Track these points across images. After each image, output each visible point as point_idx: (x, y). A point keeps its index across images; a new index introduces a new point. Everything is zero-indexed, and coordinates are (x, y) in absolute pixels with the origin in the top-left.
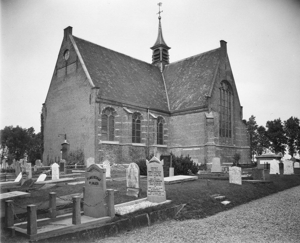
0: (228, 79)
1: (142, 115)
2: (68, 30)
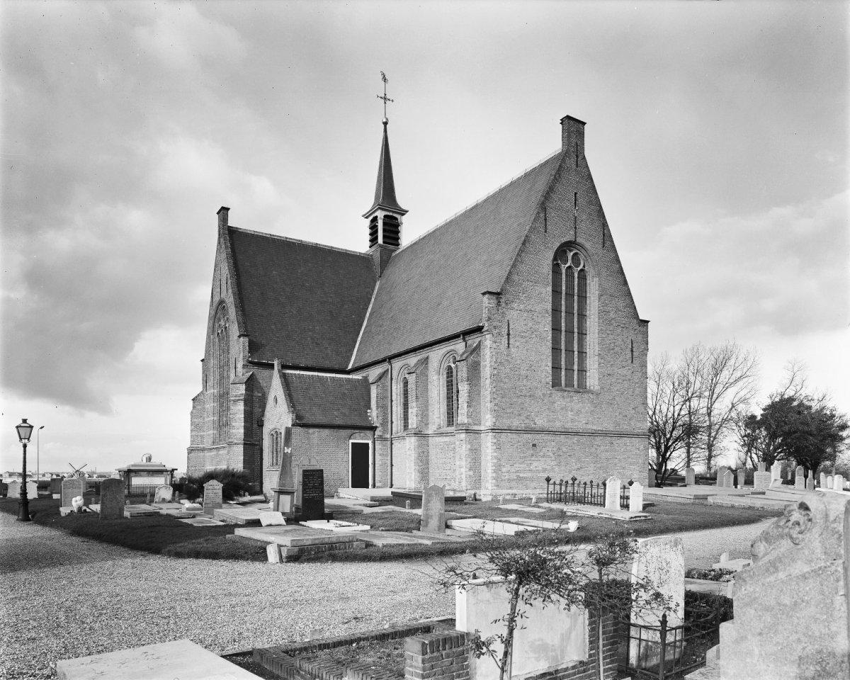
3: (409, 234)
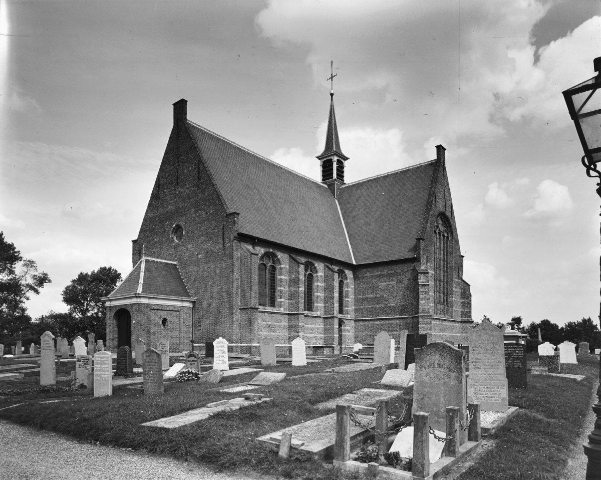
0: (448, 213)
2: (180, 107)
3: (351, 176)
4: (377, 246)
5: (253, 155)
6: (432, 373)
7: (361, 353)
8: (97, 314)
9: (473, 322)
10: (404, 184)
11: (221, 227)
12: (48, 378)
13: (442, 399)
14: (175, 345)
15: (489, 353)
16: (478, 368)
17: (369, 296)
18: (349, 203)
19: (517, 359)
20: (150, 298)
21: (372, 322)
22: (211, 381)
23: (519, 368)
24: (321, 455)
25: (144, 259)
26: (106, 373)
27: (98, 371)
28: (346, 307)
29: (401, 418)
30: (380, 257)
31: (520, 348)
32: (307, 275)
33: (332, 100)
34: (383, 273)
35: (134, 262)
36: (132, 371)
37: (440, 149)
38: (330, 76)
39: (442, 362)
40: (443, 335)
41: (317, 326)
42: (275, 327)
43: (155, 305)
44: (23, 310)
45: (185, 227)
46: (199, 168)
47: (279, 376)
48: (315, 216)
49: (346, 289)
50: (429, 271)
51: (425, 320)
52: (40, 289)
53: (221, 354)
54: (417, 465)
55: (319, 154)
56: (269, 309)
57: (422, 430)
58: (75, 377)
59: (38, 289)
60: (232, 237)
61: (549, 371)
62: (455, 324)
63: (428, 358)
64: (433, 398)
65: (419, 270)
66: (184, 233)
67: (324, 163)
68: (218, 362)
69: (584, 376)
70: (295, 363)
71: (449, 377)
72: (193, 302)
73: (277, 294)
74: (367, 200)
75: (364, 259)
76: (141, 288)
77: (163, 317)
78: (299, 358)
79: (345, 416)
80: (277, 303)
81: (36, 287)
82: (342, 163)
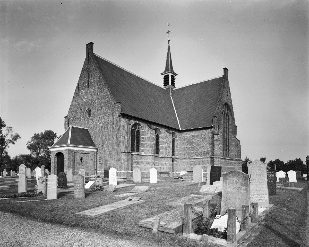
0: (229, 104)
1: (161, 130)
2: (90, 46)
3: (179, 84)
4: (192, 120)
5: (128, 73)
6: (232, 187)
7: (184, 176)
8: (44, 155)
9: (241, 160)
10: (207, 88)
11: (112, 110)
12: (22, 189)
13: (237, 201)
14: (87, 172)
15: (259, 176)
16: (253, 184)
17: (188, 146)
18: (178, 98)
19: (271, 179)
20: (74, 147)
21: (190, 160)
22: (109, 190)
23: (272, 184)
24: (176, 230)
25: (70, 126)
26: (54, 186)
27: (49, 185)
28: (176, 152)
29: (216, 211)
30: (193, 126)
31: (272, 173)
32: (156, 135)
33: (169, 43)
34: (195, 135)
35: (65, 128)
36: (66, 185)
37: (226, 70)
38: (168, 31)
39: (237, 181)
40: (226, 167)
41: (161, 162)
42: (139, 162)
43: (77, 150)
44: (7, 153)
45: (92, 110)
46: (100, 79)
47: (146, 188)
48: (160, 105)
49: (176, 143)
50: (220, 134)
51: (217, 159)
52: (15, 142)
53: (113, 176)
54: (229, 236)
55: (162, 72)
56: (137, 153)
57: (232, 217)
58: (37, 188)
59: (14, 142)
60: (117, 115)
61: (285, 186)
62: (232, 161)
63: (230, 178)
64: (233, 200)
65: (214, 133)
66: (92, 113)
67: (165, 76)
68: (112, 180)
69: (302, 188)
70: (151, 182)
71: (241, 188)
72: (97, 149)
73: (140, 145)
74: (187, 96)
75: (186, 127)
76: (70, 141)
77: (81, 157)
78: (154, 179)
79: (189, 209)
80: (140, 150)
81: (13, 141)
82: (174, 77)
